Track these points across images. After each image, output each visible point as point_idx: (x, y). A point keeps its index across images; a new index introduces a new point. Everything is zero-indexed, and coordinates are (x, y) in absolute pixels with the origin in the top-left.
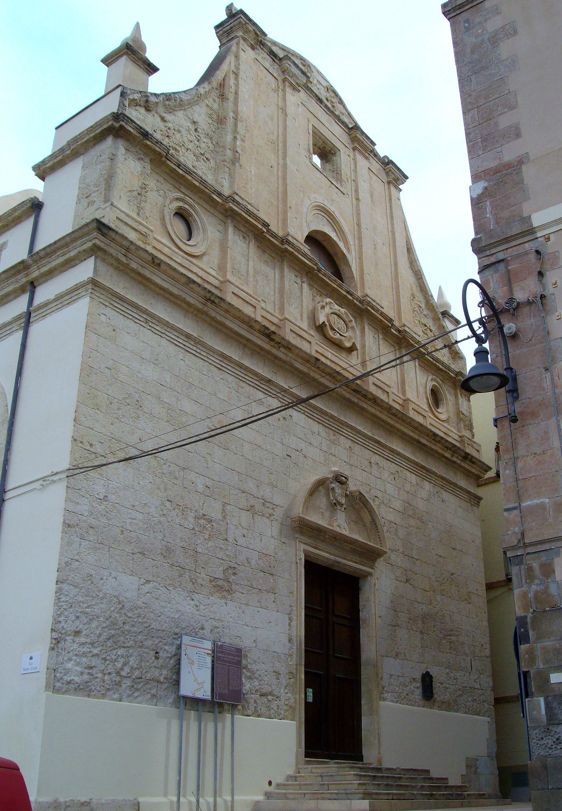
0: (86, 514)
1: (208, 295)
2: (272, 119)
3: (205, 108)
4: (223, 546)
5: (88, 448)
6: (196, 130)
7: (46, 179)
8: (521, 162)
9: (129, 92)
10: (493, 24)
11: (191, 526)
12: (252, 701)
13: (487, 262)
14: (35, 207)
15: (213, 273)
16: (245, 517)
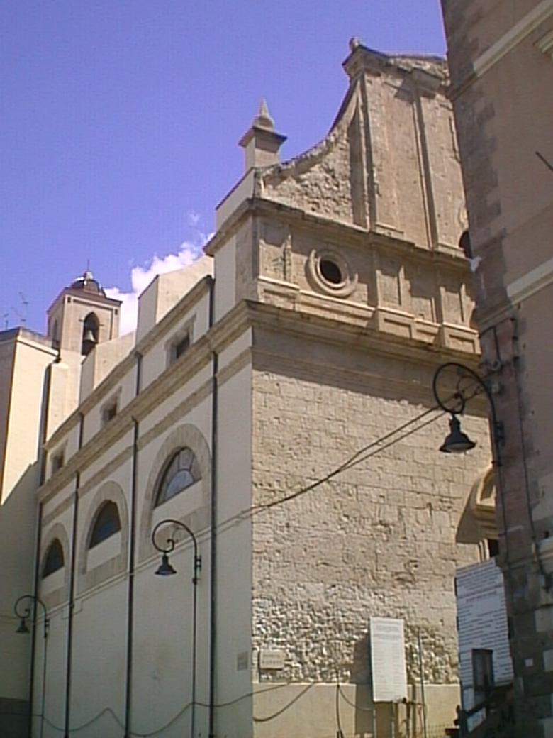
0: (272, 540)
1: (360, 330)
2: (409, 135)
3: (340, 151)
4: (402, 544)
5: (268, 488)
6: (333, 177)
7: (216, 255)
8: (502, 236)
9: (261, 170)
10: (480, 106)
11: (369, 533)
12: (443, 671)
13: (482, 330)
14: (209, 282)
15: (365, 306)
16: (423, 515)
